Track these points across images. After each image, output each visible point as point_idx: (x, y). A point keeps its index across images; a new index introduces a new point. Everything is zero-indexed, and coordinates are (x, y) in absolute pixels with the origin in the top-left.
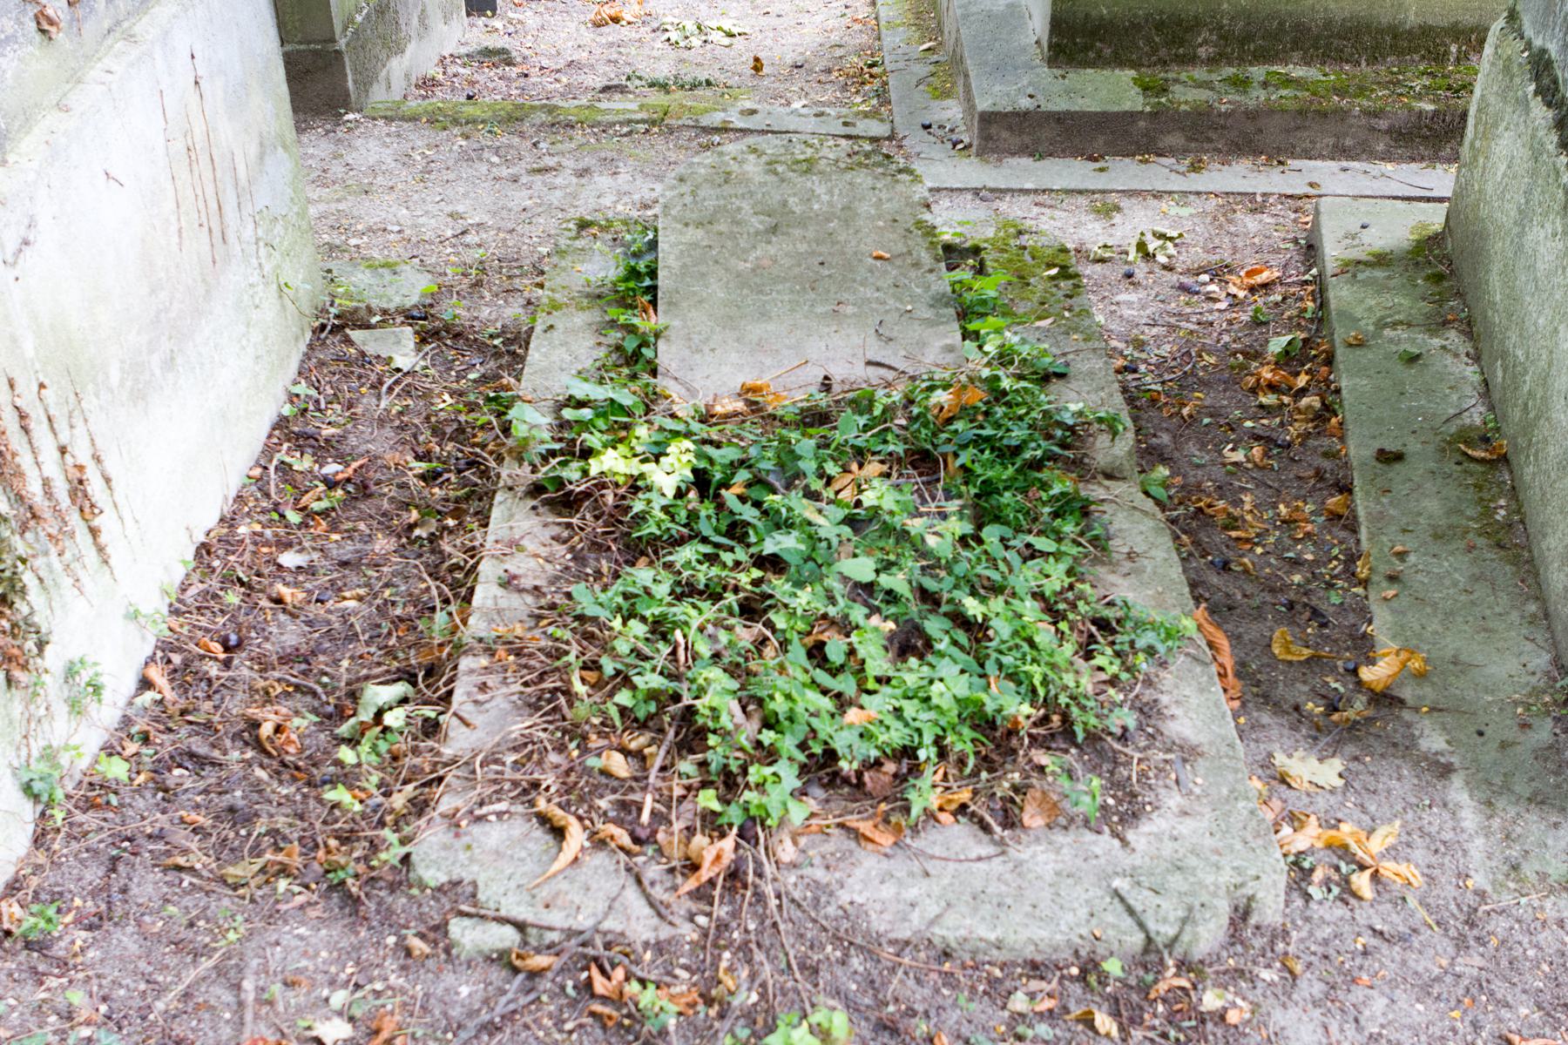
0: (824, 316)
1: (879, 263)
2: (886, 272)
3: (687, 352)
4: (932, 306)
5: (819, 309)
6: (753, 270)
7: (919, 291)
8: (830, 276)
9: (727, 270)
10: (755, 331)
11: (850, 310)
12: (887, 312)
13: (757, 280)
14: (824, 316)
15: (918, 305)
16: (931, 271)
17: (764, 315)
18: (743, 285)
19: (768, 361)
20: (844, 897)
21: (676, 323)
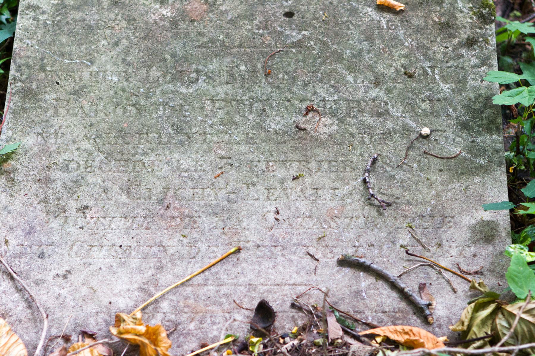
0: (280, 138)
1: (384, 19)
2: (395, 41)
3: (39, 212)
4: (464, 126)
5: (275, 123)
6: (174, 23)
7: (445, 87)
8: (298, 44)
9: (130, 20)
10: (163, 167)
11: (325, 126)
12: (388, 134)
13: (177, 47)
14: (280, 138)
15: (442, 123)
16: (470, 43)
17: (181, 134)
18: (153, 57)
19: (174, 244)
20: (6, 283)
21: (30, 141)
